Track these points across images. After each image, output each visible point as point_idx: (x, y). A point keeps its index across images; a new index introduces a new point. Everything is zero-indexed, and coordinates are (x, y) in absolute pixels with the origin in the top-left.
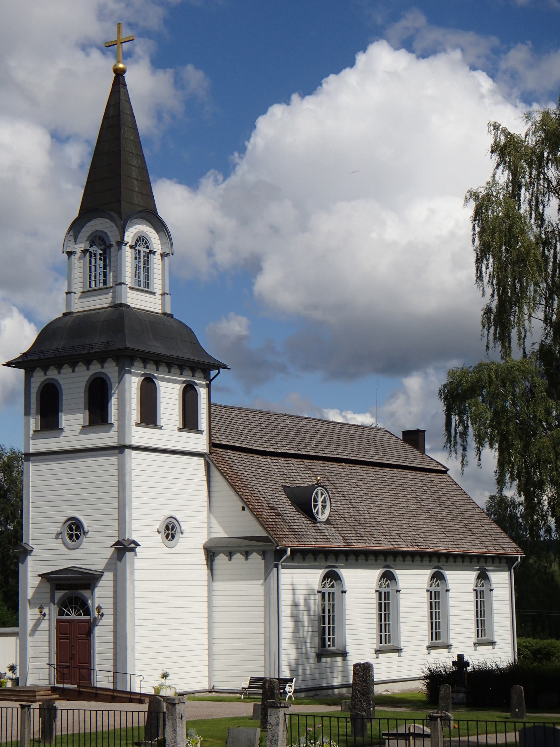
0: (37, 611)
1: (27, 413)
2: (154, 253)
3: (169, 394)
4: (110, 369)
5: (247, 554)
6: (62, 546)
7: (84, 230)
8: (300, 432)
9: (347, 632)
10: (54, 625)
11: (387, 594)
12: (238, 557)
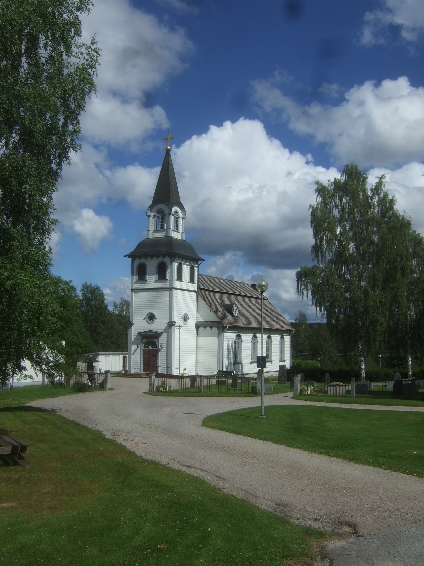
0: (136, 346)
1: (133, 274)
2: (179, 217)
3: (186, 269)
4: (167, 260)
5: (211, 328)
6: (146, 323)
7: (154, 208)
9: (243, 356)
10: (142, 351)
11: (238, 342)
12: (208, 329)
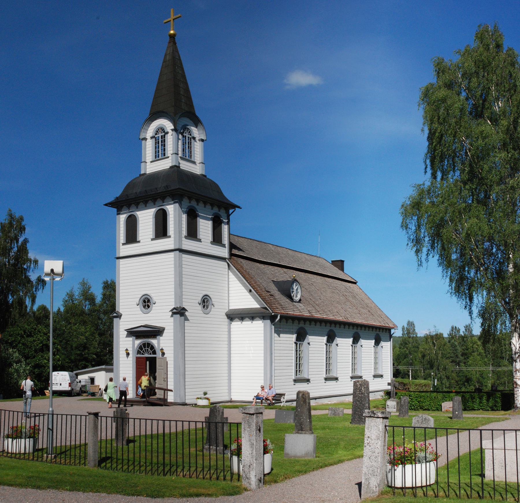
2: (194, 138)
8: (279, 253)
